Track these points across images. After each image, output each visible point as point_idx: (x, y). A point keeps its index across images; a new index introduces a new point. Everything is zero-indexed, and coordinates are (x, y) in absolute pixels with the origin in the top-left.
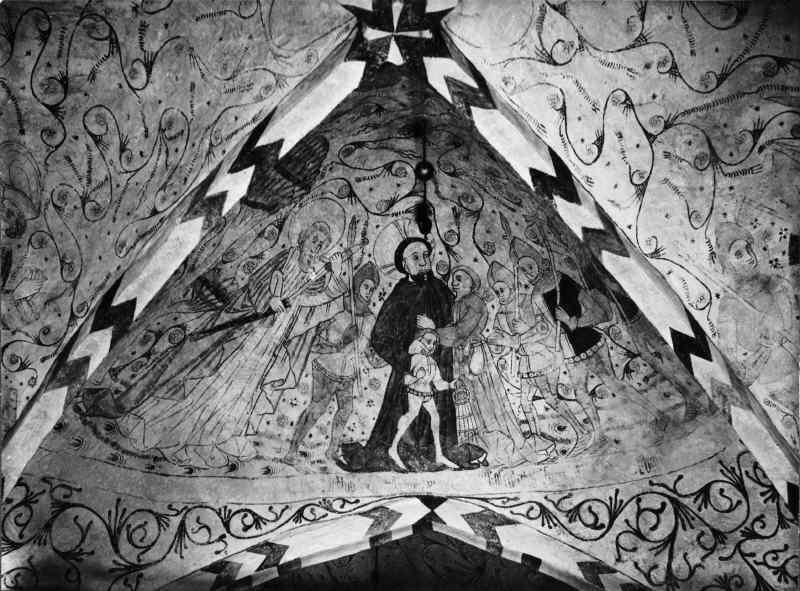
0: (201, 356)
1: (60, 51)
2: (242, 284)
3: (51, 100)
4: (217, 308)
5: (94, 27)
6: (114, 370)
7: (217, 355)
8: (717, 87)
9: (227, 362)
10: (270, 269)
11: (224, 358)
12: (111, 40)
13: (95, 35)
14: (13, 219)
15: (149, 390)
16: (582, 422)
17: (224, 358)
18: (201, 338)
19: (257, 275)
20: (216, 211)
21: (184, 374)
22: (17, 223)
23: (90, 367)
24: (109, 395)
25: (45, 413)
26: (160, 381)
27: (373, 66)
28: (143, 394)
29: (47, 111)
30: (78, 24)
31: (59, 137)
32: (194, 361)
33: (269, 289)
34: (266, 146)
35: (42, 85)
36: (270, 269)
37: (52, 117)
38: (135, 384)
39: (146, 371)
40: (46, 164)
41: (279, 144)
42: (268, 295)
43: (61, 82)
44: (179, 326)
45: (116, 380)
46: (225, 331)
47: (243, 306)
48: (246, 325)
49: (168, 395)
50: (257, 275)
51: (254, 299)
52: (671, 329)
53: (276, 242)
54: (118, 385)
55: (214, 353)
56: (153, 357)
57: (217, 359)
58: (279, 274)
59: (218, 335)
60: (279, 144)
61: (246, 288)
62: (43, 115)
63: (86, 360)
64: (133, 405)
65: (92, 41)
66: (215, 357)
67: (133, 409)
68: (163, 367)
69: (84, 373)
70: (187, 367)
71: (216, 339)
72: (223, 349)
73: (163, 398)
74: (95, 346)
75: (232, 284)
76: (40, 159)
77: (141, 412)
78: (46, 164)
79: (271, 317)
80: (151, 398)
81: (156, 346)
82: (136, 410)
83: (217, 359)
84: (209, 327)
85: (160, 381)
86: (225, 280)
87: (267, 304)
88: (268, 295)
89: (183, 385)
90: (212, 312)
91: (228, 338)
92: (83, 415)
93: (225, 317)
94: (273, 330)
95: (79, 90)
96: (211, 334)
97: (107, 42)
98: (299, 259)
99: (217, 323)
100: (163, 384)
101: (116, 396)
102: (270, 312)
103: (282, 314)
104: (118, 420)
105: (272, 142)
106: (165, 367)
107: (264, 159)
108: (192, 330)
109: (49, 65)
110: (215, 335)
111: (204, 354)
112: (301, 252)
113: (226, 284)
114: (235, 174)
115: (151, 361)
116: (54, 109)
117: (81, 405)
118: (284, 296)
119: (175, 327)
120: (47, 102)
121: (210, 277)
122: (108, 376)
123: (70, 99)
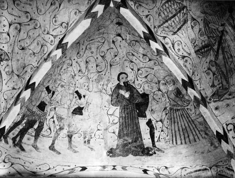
0: (224, 59)
1: (136, 53)
2: (207, 38)
3: (148, 60)
4: (211, 49)
5: (133, 44)
6: (212, 86)
7: (227, 54)
8: (30, 21)
9: (231, 52)
10: (207, 27)
11: (229, 52)
12: (136, 42)
13: (134, 44)
14: (171, 81)
15: (226, 78)
16: (104, 88)
17: (229, 52)
18: (218, 57)
19: (206, 32)
20: (161, 52)
21: (227, 66)
22: (173, 81)
23: (197, 96)
24: (219, 90)
25: (204, 112)
26: (226, 74)
27: (122, 5)
28: (226, 80)
29: (150, 62)
30: (131, 47)
31: (156, 62)
32: (225, 62)
33: (214, 29)
34: (144, 36)
35: (144, 60)
36: (207, 27)
37: (152, 61)
38: (222, 81)
39: (220, 77)
40: (162, 67)
41: (144, 33)
42: (216, 30)
43: (144, 56)
44: (210, 62)
45: (216, 86)
46: (220, 48)
47: (215, 40)
48: (222, 41)
49: (231, 73)
50: (206, 32)
51: (215, 35)
52: (5, 126)
53: (199, 22)
54: (218, 86)
55: (226, 55)
56: (216, 73)
57: (228, 54)
58: (211, 24)
59: (220, 52)
60: (144, 33)
61: (209, 37)
62: (150, 63)
63: (195, 97)
64: (228, 85)
65: (136, 46)
66: (227, 55)
67: (229, 86)
68: (221, 71)
69: (198, 99)
70: (225, 65)
71: (221, 52)
72: (226, 51)
73: (231, 76)
74: (191, 93)
75: (204, 42)
76: (161, 68)
77: (232, 84)
78: (162, 67)
79: (224, 32)
80: (229, 79)
81: (213, 71)
82: (230, 85)
83: (228, 54)
84: (216, 54)
85: (226, 74)
86: (202, 44)
87: (219, 32)
88: (216, 30)
89: (231, 68)
90: (211, 50)
91: (223, 49)
92: (219, 101)
93: (216, 47)
94: (229, 33)
95: (147, 53)
96: (219, 54)
97: (136, 43)
98: (210, 15)
99: (216, 50)
100: (227, 74)
101: (221, 88)
102: (222, 32)
103: (226, 28)
104: (229, 91)
105: (143, 34)
106: (221, 71)
107: (148, 37)
108: (214, 59)
109: (139, 57)
110: (220, 53)
111: (224, 58)
112: (208, 13)
113: (203, 44)
114: (151, 45)
115: (217, 74)
116: (150, 60)
117: (215, 100)
118: (220, 25)
119: (209, 64)
120: (148, 61)
121: (197, 49)
122: (212, 88)
123: (148, 55)
